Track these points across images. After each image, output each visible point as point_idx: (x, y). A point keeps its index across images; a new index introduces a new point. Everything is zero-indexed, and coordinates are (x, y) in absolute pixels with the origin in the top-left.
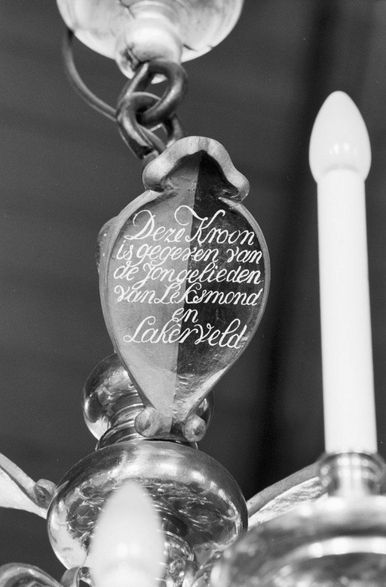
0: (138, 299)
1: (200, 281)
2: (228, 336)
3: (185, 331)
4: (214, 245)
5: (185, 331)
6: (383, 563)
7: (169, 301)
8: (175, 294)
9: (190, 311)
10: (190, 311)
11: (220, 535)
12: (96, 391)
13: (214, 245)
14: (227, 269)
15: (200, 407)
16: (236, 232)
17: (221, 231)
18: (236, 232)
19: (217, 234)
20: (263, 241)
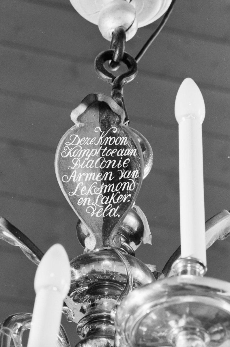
0: (109, 209)
1: (80, 144)
2: (106, 151)
3: (105, 139)
4: (110, 169)
5: (105, 139)
6: (115, 346)
7: (81, 194)
8: (100, 210)
9: (107, 174)
10: (107, 174)
11: (109, 235)
12: (114, 84)
13: (110, 169)
14: (94, 145)
15: (110, 254)
16: (106, 216)
17: (111, 138)
18: (106, 216)
19: (109, 140)
20: (64, 136)
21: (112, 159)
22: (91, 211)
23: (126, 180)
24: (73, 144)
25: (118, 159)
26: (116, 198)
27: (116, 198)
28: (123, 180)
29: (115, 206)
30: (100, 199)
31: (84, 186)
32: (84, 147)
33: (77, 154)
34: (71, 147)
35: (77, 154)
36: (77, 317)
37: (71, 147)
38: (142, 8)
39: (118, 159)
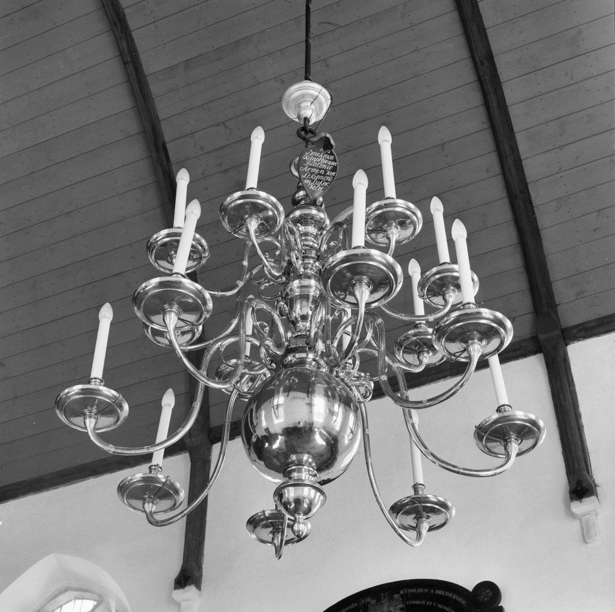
4: (323, 169)
21: (325, 164)
22: (310, 186)
23: (329, 176)
24: (415, 503)
25: (328, 165)
26: (322, 183)
27: (322, 183)
28: (328, 175)
29: (321, 186)
30: (316, 182)
31: (316, 494)
32: (314, 156)
33: (447, 594)
34: (307, 155)
35: (447, 594)
36: (260, 514)
37: (307, 155)
38: (262, 255)
39: (328, 165)
